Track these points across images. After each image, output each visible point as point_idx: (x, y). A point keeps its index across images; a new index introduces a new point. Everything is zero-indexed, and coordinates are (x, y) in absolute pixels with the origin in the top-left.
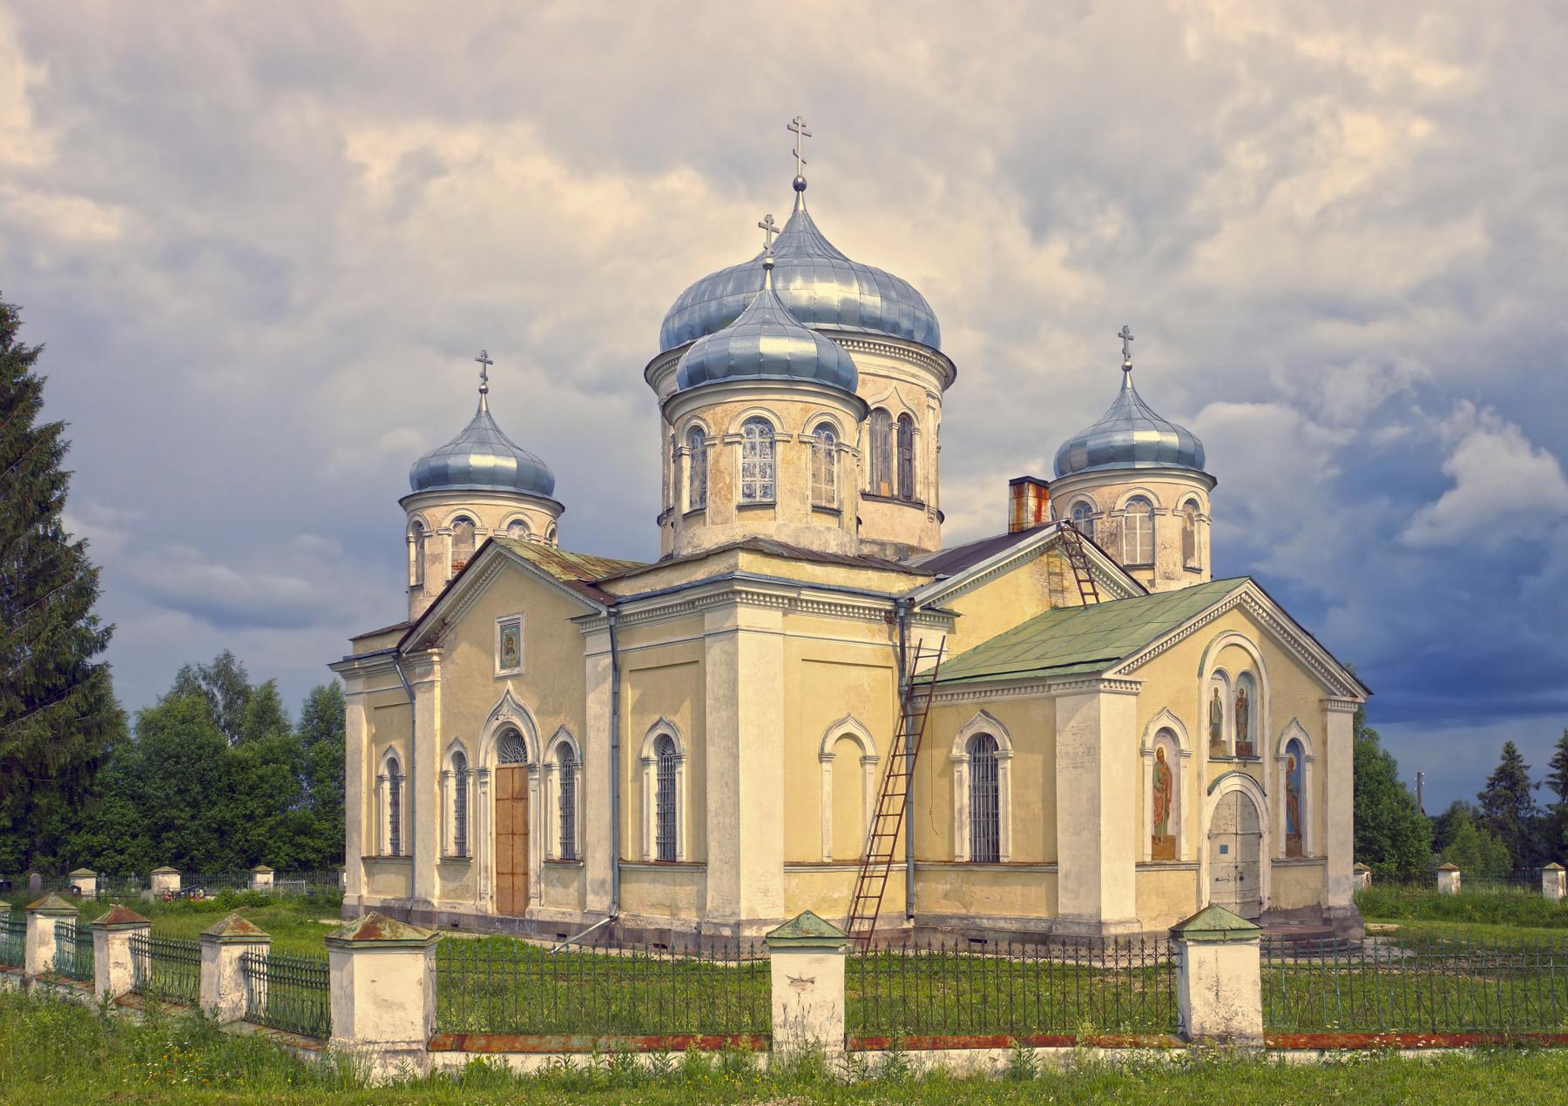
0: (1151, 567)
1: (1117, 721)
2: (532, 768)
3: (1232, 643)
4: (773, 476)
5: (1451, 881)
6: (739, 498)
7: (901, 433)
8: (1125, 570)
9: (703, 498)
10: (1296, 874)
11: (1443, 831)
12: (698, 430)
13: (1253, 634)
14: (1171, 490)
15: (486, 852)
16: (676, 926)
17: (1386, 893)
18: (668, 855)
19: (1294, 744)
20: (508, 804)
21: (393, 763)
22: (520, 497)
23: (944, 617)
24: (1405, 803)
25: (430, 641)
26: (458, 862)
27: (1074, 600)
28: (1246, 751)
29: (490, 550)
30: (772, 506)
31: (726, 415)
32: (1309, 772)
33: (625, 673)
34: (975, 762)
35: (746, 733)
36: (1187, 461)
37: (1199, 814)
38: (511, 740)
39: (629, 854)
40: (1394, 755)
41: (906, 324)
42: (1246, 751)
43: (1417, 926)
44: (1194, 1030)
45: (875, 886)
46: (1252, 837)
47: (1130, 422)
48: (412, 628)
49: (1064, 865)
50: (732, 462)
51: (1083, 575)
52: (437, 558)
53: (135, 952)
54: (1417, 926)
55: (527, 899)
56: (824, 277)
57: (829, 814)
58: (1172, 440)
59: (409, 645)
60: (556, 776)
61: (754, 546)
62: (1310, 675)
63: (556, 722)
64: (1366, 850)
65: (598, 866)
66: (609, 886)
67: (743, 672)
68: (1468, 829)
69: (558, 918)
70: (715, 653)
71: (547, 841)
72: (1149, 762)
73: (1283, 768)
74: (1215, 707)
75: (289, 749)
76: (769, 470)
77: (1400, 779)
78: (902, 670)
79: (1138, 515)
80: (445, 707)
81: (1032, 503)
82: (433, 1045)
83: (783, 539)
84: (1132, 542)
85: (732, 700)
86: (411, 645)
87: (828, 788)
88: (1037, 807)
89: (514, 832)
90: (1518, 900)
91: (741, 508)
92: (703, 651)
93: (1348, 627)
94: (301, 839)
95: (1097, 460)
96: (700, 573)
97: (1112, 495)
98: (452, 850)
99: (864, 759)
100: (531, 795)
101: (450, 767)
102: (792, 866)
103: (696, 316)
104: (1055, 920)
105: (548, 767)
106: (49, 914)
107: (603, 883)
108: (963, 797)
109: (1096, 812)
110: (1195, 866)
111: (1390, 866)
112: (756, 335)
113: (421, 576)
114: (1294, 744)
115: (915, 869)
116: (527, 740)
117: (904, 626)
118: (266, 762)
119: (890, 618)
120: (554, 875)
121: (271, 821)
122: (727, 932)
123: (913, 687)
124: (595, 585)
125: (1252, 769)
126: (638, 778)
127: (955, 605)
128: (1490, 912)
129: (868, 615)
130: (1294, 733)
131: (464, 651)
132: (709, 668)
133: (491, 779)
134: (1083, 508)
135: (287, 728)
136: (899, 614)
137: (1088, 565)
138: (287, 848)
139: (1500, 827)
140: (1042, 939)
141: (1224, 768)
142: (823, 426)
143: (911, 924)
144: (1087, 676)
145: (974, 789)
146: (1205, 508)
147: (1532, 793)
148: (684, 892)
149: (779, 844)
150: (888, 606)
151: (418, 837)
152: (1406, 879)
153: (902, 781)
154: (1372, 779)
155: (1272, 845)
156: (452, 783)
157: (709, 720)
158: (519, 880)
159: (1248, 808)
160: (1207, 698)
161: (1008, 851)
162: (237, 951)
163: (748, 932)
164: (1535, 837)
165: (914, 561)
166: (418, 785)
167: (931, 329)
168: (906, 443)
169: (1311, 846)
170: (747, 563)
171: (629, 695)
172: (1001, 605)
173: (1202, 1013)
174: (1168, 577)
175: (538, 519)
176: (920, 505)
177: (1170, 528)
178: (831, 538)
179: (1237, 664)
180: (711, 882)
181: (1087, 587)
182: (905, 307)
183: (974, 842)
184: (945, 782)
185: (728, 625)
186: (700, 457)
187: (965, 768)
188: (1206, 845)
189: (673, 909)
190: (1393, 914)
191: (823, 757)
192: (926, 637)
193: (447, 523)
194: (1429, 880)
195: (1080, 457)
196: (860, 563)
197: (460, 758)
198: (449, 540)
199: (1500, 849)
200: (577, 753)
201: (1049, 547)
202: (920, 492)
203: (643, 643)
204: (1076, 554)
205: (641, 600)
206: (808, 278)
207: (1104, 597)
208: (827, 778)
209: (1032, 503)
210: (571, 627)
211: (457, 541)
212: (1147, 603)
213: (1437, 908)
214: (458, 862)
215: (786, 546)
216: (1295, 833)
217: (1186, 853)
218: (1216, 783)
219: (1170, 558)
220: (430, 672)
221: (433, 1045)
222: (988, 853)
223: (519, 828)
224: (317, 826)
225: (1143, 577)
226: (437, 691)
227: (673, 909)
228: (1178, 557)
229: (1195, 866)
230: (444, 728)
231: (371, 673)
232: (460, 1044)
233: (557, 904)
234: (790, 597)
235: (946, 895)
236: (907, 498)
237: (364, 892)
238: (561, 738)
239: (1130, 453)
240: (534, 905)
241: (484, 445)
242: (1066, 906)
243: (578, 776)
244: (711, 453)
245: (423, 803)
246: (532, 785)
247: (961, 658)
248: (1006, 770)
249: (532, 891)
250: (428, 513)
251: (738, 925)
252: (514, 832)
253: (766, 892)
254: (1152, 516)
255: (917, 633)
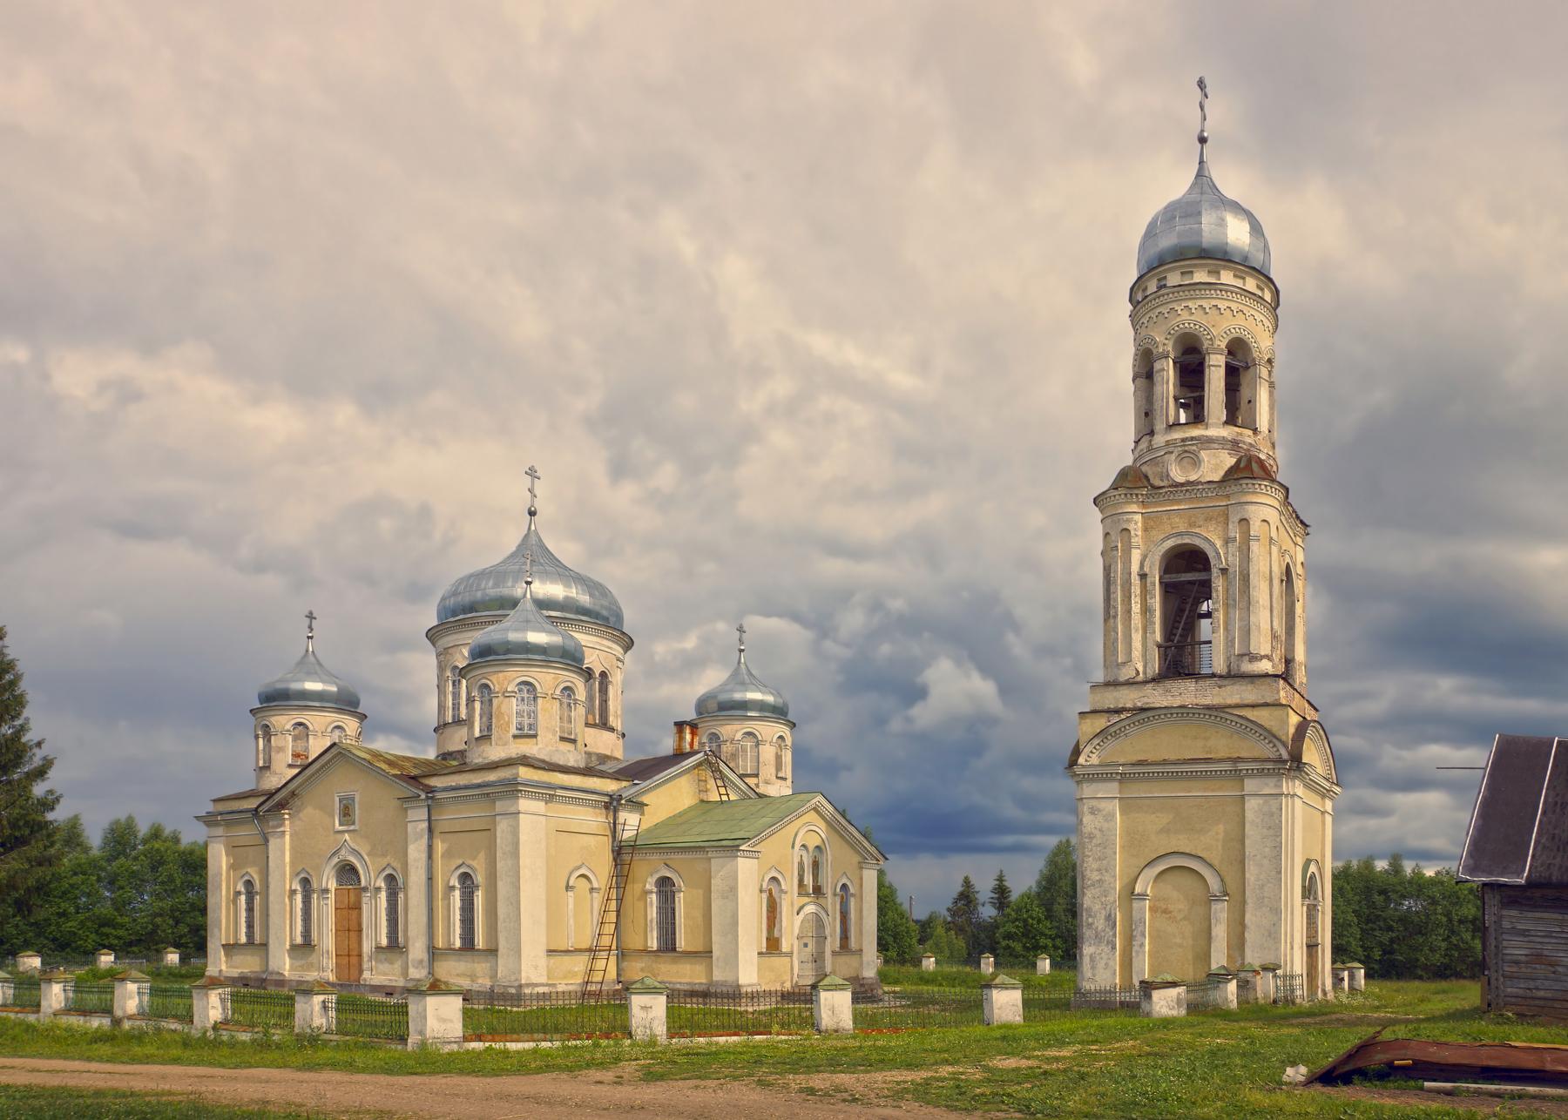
0: (757, 776)
1: (747, 871)
2: (365, 889)
3: (809, 829)
4: (536, 718)
5: (929, 963)
6: (514, 731)
7: (601, 683)
8: (741, 777)
9: (489, 728)
10: (843, 959)
11: (926, 927)
12: (486, 686)
13: (822, 825)
14: (771, 730)
15: (327, 940)
16: (475, 987)
17: (892, 969)
18: (468, 943)
19: (844, 886)
20: (345, 912)
21: (249, 884)
22: (340, 711)
23: (638, 806)
24: (902, 916)
25: (282, 805)
26: (306, 946)
27: (714, 797)
28: (818, 890)
29: (334, 751)
30: (535, 736)
31: (506, 679)
32: (853, 903)
33: (436, 833)
34: (659, 893)
35: (525, 873)
36: (778, 712)
37: (792, 926)
38: (347, 872)
39: (440, 943)
40: (895, 885)
41: (605, 613)
42: (818, 890)
43: (910, 988)
44: (823, 1027)
45: (600, 964)
46: (821, 939)
47: (744, 686)
48: (271, 795)
49: (716, 953)
50: (510, 709)
51: (720, 783)
52: (281, 749)
53: (222, 1001)
54: (910, 988)
55: (361, 972)
56: (553, 581)
57: (571, 922)
58: (770, 699)
59: (265, 807)
60: (383, 895)
61: (525, 761)
62: (842, 836)
63: (384, 862)
64: (882, 946)
65: (418, 950)
66: (426, 963)
67: (523, 838)
68: (940, 931)
69: (386, 983)
70: (502, 826)
71: (376, 932)
72: (765, 896)
73: (838, 900)
74: (801, 865)
75: (94, 864)
76: (533, 714)
77: (899, 901)
78: (614, 837)
79: (749, 744)
80: (292, 848)
81: (688, 737)
82: (466, 1039)
83: (541, 756)
84: (745, 760)
85: (515, 854)
86: (269, 806)
87: (571, 906)
88: (700, 919)
89: (350, 926)
90: (968, 974)
91: (515, 737)
92: (494, 823)
93: (859, 783)
94: (106, 930)
95: (720, 707)
96: (492, 777)
97: (732, 731)
98: (299, 940)
99: (592, 890)
100: (364, 907)
101: (297, 886)
102: (551, 952)
103: (466, 598)
104: (711, 983)
105: (378, 889)
106: (134, 981)
107: (421, 961)
108: (653, 913)
109: (736, 923)
110: (790, 955)
111: (893, 954)
112: (525, 630)
113: (268, 760)
114: (844, 886)
115: (623, 955)
116: (361, 872)
117: (615, 811)
118: (75, 874)
119: (607, 806)
120: (382, 956)
121: (81, 917)
122: (513, 991)
123: (621, 848)
124: (414, 778)
125: (821, 901)
126: (447, 897)
127: (645, 799)
128: (952, 980)
129: (594, 805)
130: (844, 881)
131: (309, 813)
132: (499, 834)
133: (332, 896)
134: (714, 737)
135: (86, 850)
136: (612, 804)
137: (723, 777)
138: (93, 936)
139: (960, 930)
140: (705, 995)
141: (806, 900)
142: (566, 688)
143: (619, 986)
144: (731, 848)
145: (659, 908)
146: (789, 741)
147: (980, 908)
148: (481, 967)
149: (543, 939)
150: (606, 799)
151: (272, 932)
152: (903, 962)
153: (614, 903)
154: (886, 899)
155: (832, 943)
156: (299, 898)
157: (499, 865)
158: (354, 960)
159: (819, 923)
160: (797, 860)
161: (682, 943)
162: (321, 998)
163: (527, 991)
164: (983, 936)
165: (609, 767)
166: (271, 898)
167: (619, 617)
168: (604, 690)
169: (853, 944)
170: (524, 773)
171: (440, 847)
172: (671, 798)
173: (826, 1021)
174: (767, 783)
175: (351, 725)
176: (612, 730)
177: (768, 753)
178: (572, 757)
179: (813, 841)
180: (500, 961)
181: (723, 791)
182: (605, 603)
183: (659, 939)
184: (640, 905)
185: (512, 810)
186: (488, 703)
187: (654, 896)
188: (796, 942)
189: (473, 977)
190: (896, 982)
191: (568, 888)
192: (631, 822)
193: (288, 727)
194: (917, 962)
195: (713, 705)
196: (587, 772)
197: (306, 882)
198: (290, 738)
199: (960, 943)
200: (400, 882)
201: (700, 764)
202: (612, 721)
203: (450, 816)
204: (716, 771)
205: (448, 784)
206: (543, 581)
207: (733, 797)
208: (571, 901)
209: (688, 737)
210: (398, 803)
211: (295, 738)
212: (760, 803)
213: (921, 979)
214: (306, 946)
215: (543, 761)
216: (845, 937)
217: (785, 947)
218: (801, 908)
219: (768, 771)
220: (282, 825)
221: (466, 1039)
222: (668, 945)
223: (354, 925)
224: (119, 920)
225: (752, 781)
226: (287, 837)
227: (473, 977)
228: (773, 771)
229: (790, 955)
230: (293, 863)
231: (229, 824)
232: (479, 1038)
233: (385, 974)
234: (549, 794)
235: (642, 970)
236: (604, 725)
237: (224, 967)
238: (388, 871)
239: (744, 705)
240: (366, 975)
241: (311, 675)
242: (718, 975)
243: (401, 895)
244: (495, 702)
245: (274, 911)
246: (365, 900)
247: (648, 831)
248: (680, 898)
249: (365, 965)
250: (273, 719)
251: (521, 986)
252: (350, 926)
253: (536, 967)
254: (757, 745)
255: (623, 815)
